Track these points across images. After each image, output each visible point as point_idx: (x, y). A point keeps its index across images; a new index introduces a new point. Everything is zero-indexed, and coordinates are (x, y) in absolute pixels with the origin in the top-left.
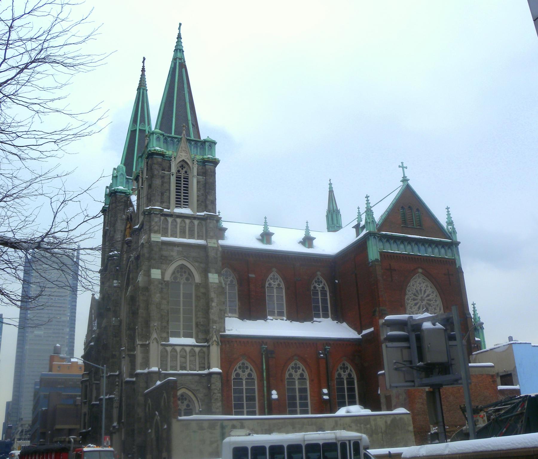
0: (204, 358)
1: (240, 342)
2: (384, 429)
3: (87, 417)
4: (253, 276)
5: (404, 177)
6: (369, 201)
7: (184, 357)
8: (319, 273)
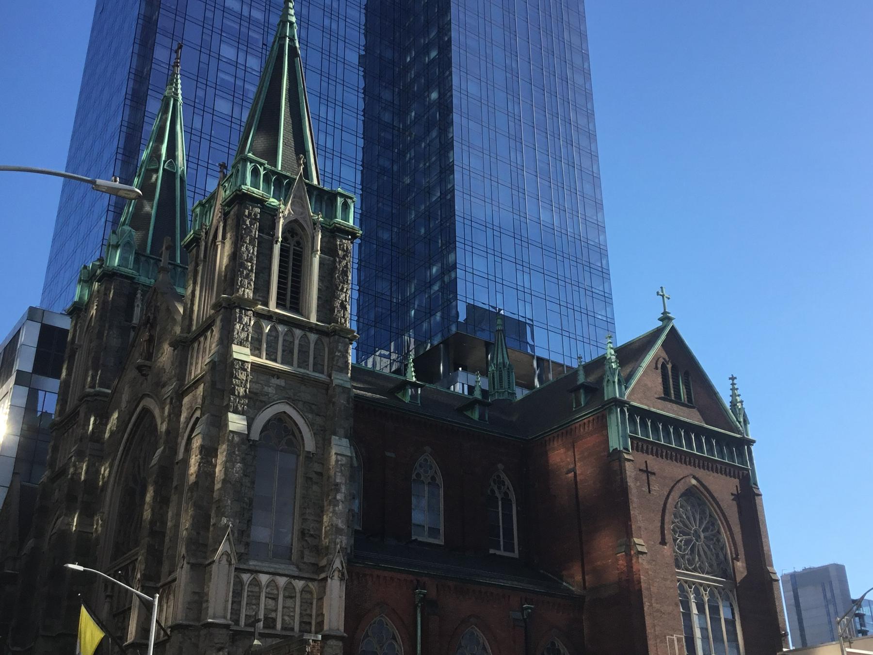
0: (312, 604)
1: (378, 576)
4: (393, 455)
5: (665, 313)
6: (736, 387)
7: (273, 599)
8: (500, 466)
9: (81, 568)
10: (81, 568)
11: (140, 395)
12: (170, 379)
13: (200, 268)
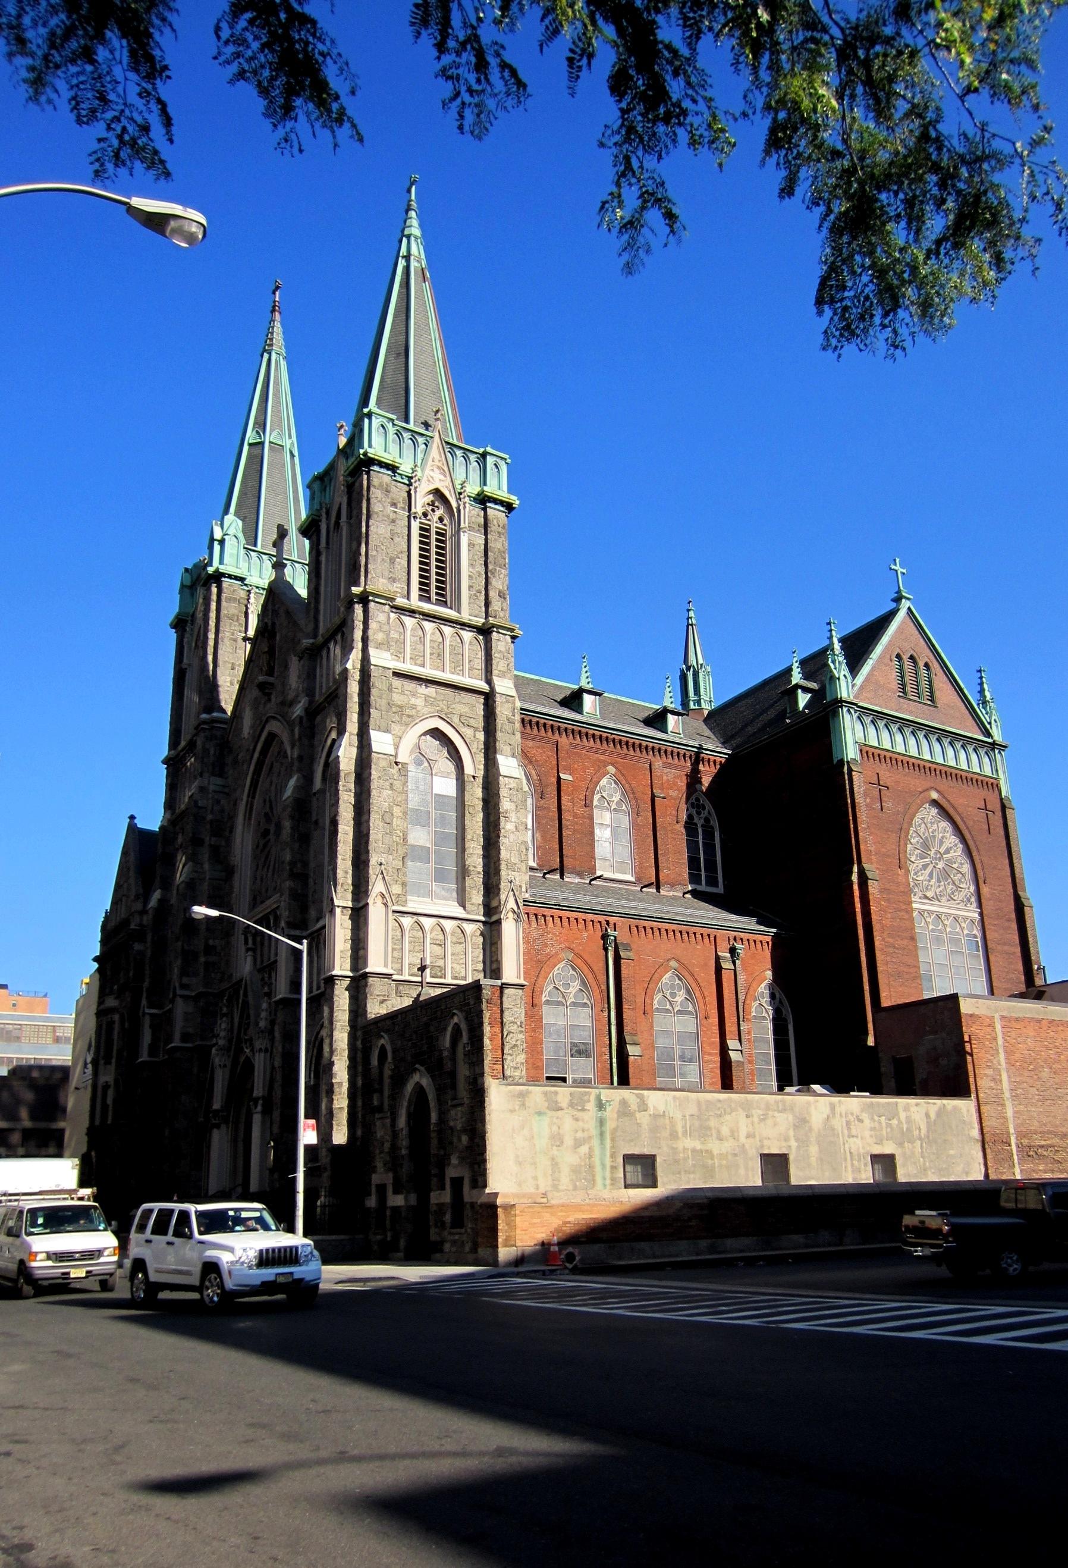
2: (924, 1131)
3: (111, 1093)
9: (214, 913)
10: (214, 913)
11: (264, 719)
12: (297, 696)
13: (323, 558)
